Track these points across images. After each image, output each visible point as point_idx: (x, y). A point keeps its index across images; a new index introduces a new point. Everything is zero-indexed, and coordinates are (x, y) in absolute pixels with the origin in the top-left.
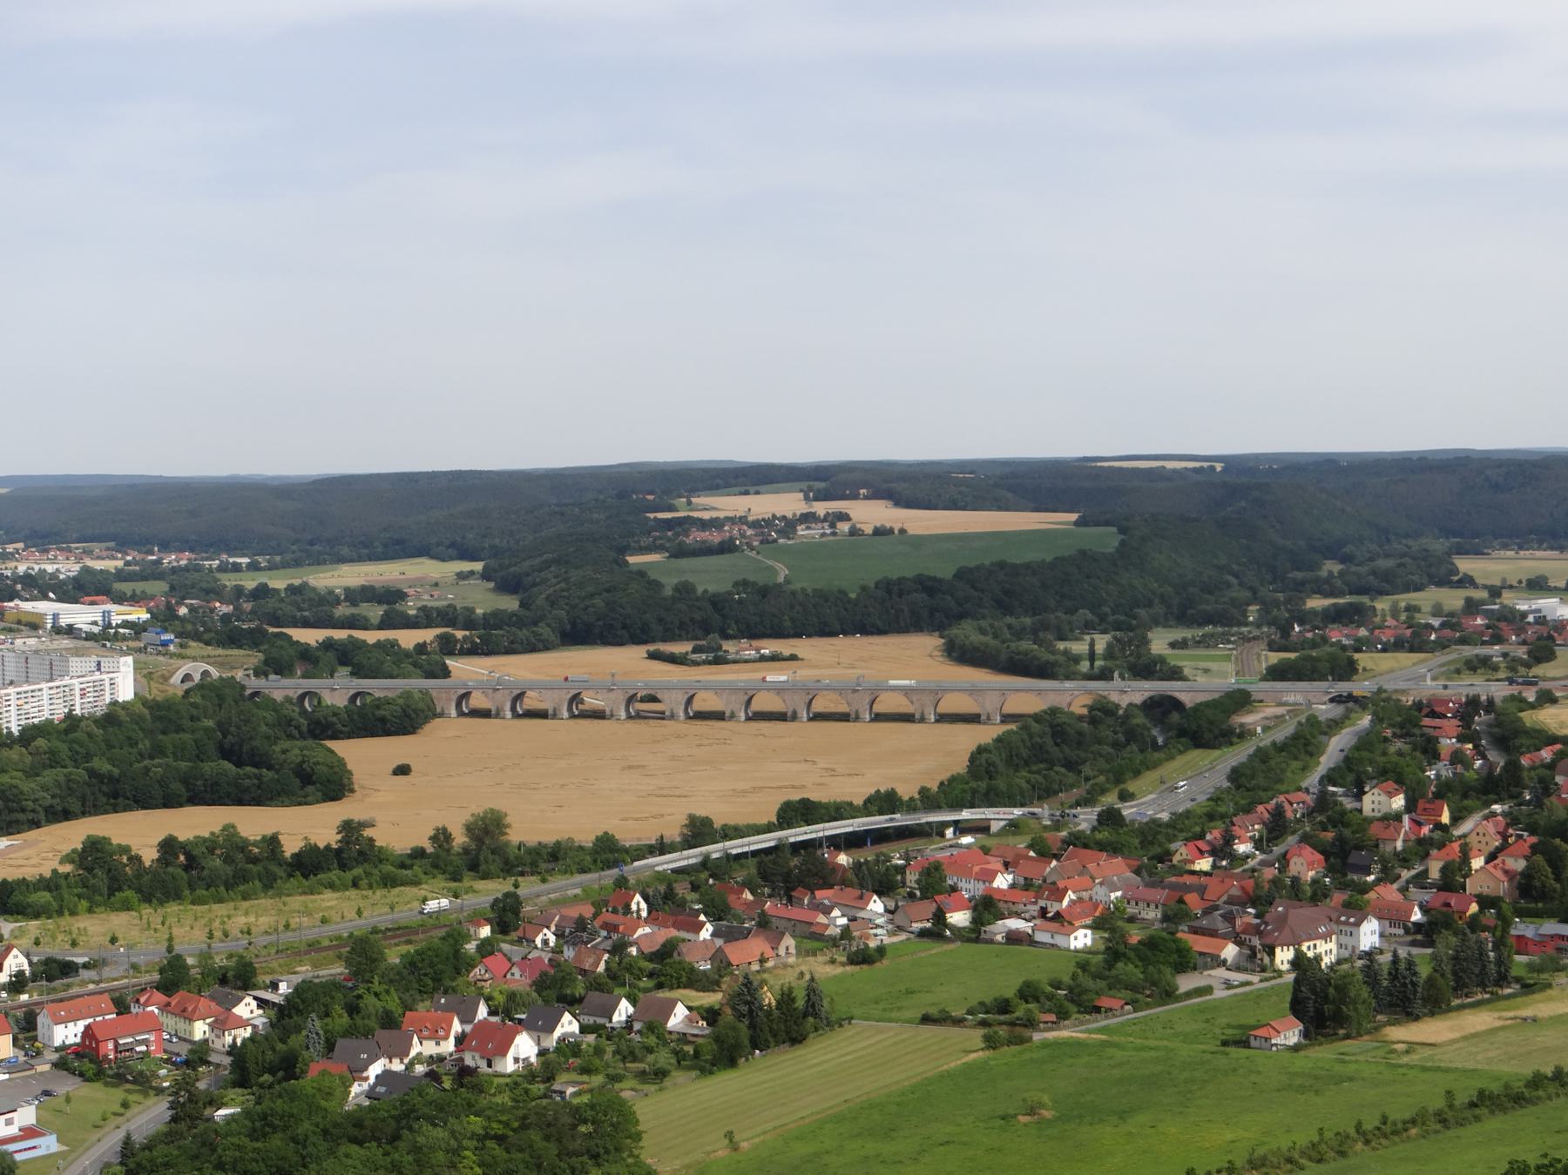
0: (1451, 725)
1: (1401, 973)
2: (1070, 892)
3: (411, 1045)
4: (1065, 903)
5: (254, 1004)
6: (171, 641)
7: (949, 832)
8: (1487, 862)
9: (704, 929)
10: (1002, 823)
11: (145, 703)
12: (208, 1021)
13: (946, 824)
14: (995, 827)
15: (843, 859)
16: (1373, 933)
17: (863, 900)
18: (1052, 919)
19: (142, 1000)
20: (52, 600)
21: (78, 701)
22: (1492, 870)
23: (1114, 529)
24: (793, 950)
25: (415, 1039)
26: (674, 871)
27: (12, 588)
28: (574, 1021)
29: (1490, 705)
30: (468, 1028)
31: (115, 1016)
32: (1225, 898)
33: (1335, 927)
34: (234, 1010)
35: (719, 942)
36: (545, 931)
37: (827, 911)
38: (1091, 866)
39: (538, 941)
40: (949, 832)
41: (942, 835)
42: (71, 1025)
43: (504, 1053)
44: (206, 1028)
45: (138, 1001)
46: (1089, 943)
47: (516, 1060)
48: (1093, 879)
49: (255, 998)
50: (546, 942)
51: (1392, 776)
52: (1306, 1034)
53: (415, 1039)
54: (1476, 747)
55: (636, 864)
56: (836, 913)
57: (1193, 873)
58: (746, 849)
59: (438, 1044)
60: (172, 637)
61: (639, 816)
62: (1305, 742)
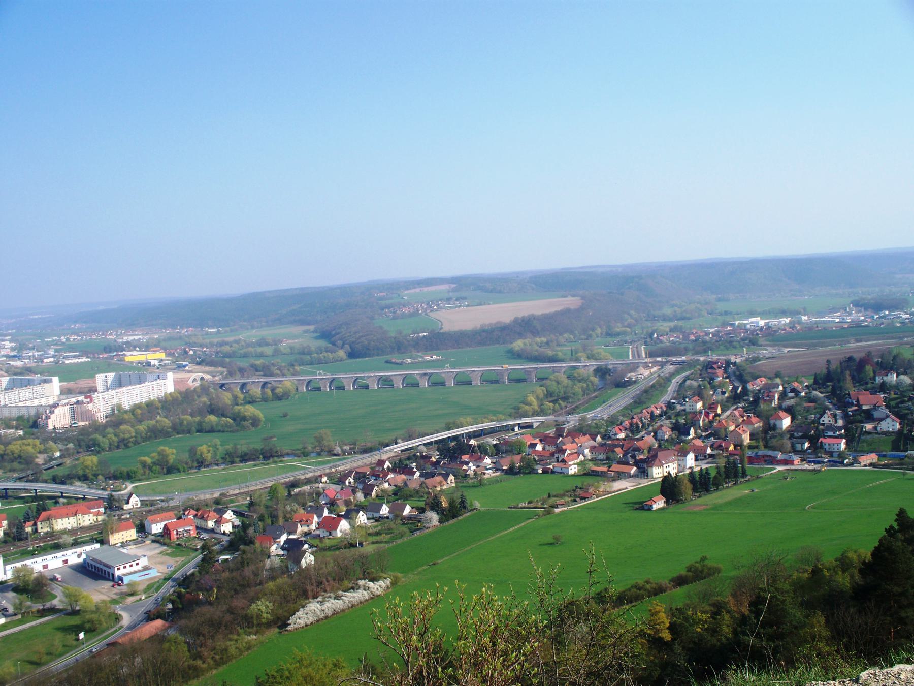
0: (720, 372)
1: (704, 474)
2: (568, 450)
3: (297, 527)
4: (566, 454)
5: (232, 513)
6: (187, 365)
7: (516, 429)
8: (736, 427)
9: (416, 475)
10: (538, 424)
11: (180, 393)
12: (214, 521)
13: (514, 425)
14: (535, 425)
15: (472, 442)
16: (692, 459)
17: (481, 459)
18: (561, 461)
19: (186, 513)
20: (137, 351)
21: (151, 392)
22: (739, 431)
23: (579, 298)
24: (453, 481)
25: (299, 525)
26: (402, 451)
27: (122, 347)
28: (364, 515)
29: (735, 364)
30: (321, 519)
31: (175, 520)
32: (631, 449)
33: (677, 458)
34: (224, 516)
35: (422, 479)
36: (350, 478)
37: (467, 464)
38: (576, 440)
39: (347, 483)
40: (516, 429)
41: (513, 430)
42: (158, 524)
43: (336, 529)
44: (213, 524)
45: (184, 514)
46: (577, 471)
47: (341, 531)
48: (577, 444)
49: (232, 511)
50: (350, 483)
51: (699, 394)
52: (667, 502)
53: (299, 525)
54: (730, 380)
55: (386, 448)
56: (471, 464)
57: (618, 439)
58: (431, 440)
59: (308, 526)
60: (188, 363)
61: (335, 457)
62: (661, 385)
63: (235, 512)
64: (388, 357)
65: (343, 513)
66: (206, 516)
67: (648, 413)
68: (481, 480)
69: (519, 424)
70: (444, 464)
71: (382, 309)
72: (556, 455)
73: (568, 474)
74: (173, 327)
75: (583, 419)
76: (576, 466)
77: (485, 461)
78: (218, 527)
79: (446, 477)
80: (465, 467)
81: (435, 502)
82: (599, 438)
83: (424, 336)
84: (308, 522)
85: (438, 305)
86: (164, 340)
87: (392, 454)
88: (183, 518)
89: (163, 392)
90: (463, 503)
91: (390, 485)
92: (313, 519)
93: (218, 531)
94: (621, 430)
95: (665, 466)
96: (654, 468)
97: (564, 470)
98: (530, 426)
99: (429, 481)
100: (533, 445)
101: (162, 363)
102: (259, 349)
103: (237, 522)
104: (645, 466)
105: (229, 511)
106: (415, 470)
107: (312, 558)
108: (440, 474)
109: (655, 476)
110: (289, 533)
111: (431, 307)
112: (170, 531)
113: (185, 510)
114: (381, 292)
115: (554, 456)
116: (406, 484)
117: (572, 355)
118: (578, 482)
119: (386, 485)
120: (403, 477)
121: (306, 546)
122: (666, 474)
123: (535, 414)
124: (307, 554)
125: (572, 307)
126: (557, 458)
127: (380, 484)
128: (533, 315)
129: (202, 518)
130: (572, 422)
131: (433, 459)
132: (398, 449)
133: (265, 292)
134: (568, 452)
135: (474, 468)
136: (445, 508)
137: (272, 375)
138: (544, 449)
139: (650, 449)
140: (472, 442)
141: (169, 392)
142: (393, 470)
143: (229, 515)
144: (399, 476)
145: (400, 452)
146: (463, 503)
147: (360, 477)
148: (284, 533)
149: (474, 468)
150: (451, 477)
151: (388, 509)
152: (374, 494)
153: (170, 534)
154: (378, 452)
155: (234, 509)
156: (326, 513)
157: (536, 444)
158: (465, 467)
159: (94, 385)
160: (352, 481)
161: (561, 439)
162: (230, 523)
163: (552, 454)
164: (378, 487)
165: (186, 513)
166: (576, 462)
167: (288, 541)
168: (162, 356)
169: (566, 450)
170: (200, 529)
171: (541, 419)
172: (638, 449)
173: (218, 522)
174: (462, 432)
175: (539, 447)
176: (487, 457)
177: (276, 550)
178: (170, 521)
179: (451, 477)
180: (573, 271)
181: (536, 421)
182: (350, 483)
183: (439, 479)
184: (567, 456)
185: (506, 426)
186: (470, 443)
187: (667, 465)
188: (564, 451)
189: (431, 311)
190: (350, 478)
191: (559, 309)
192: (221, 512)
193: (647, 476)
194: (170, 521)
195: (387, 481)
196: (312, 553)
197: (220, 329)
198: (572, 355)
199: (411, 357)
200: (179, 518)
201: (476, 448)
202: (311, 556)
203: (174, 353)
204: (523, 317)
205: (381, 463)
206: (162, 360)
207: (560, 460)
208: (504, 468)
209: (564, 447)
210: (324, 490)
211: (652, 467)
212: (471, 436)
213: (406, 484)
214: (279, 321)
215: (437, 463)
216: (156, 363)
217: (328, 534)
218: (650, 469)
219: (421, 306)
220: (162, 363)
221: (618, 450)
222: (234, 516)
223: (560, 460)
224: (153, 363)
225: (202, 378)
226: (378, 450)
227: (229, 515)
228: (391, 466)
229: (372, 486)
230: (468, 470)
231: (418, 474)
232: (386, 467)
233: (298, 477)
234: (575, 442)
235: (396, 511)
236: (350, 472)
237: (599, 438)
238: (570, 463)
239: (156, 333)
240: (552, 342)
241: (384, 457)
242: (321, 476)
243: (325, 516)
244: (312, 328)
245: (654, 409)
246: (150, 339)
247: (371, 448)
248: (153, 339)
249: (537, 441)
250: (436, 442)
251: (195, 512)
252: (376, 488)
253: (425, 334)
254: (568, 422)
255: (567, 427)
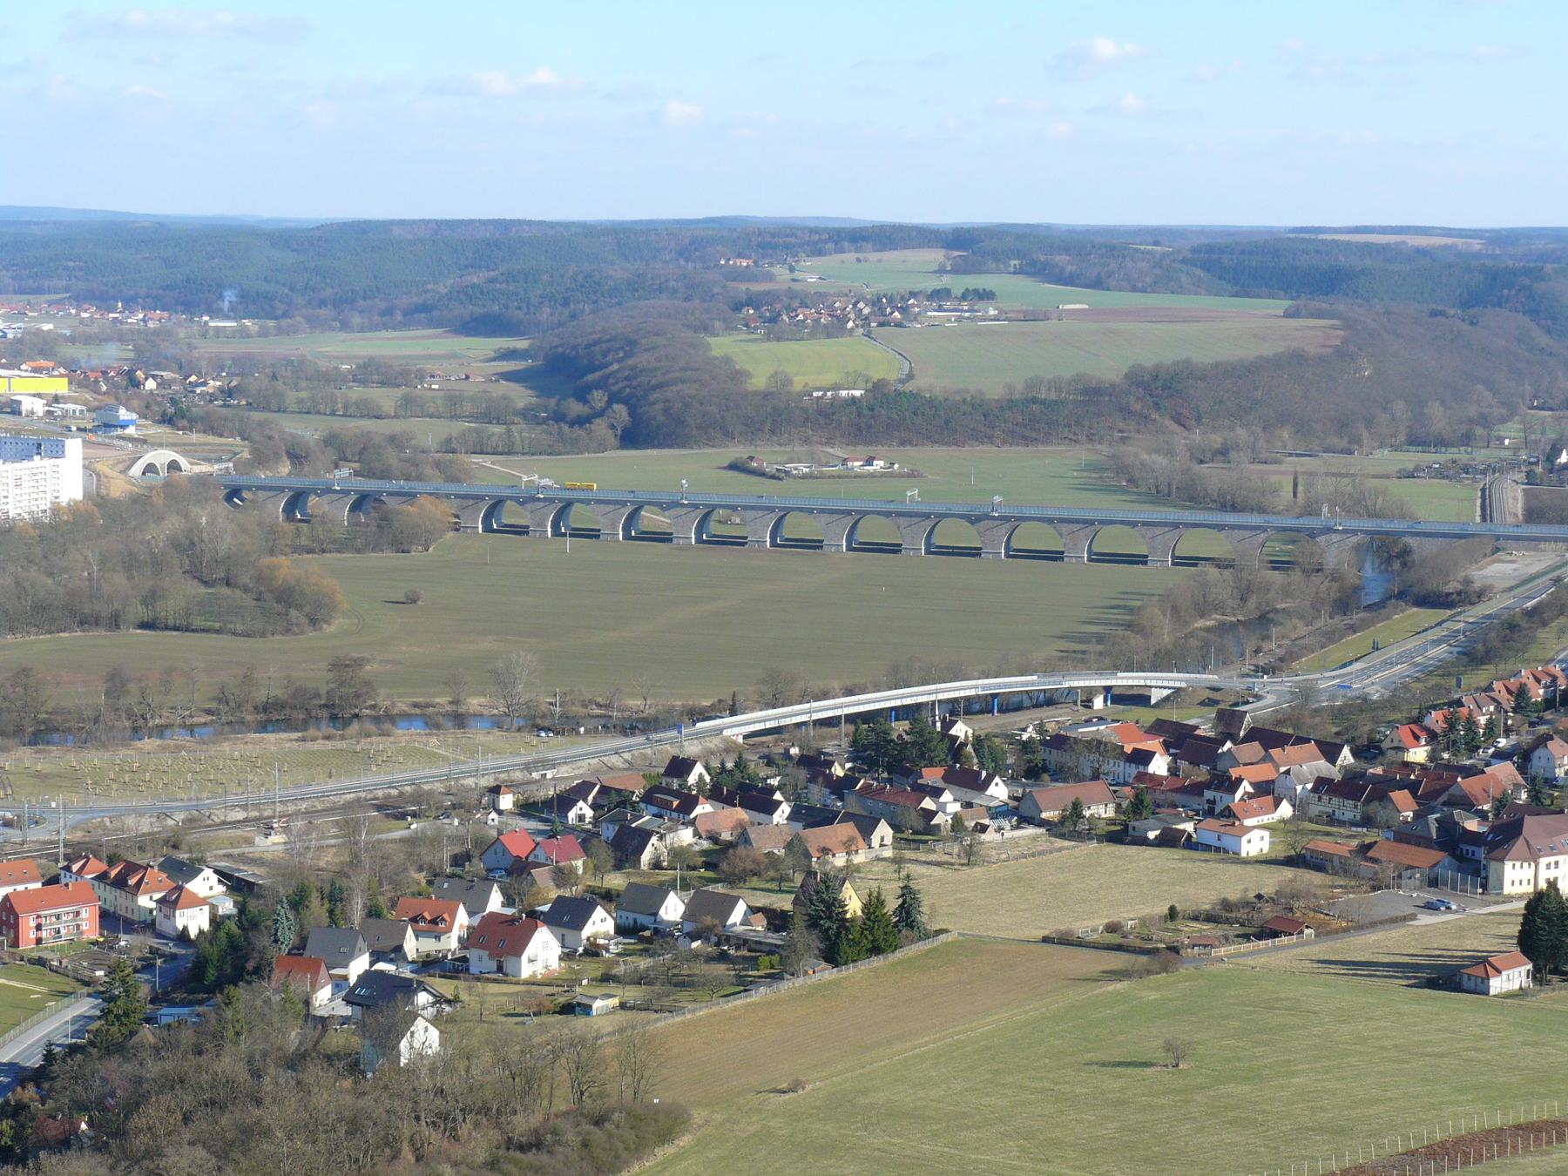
9: (779, 812)
10: (1166, 692)
12: (157, 896)
13: (1090, 693)
14: (1156, 696)
19: (75, 868)
24: (888, 840)
25: (410, 931)
30: (476, 920)
31: (39, 885)
37: (936, 793)
40: (1098, 703)
41: (1087, 703)
45: (68, 869)
48: (1277, 767)
49: (216, 871)
52: (1537, 975)
53: (410, 931)
56: (947, 797)
63: (223, 875)
64: (736, 452)
65: (546, 908)
66: (132, 881)
67: (1509, 692)
68: (971, 846)
69: (1107, 689)
70: (867, 787)
71: (738, 308)
72: (1208, 794)
73: (1237, 853)
74: (103, 300)
75: (1305, 694)
76: (1266, 834)
77: (992, 790)
78: (167, 917)
79: (867, 828)
80: (928, 803)
81: (823, 901)
82: (1346, 756)
83: (853, 398)
84: (435, 925)
85: (903, 310)
86: (72, 340)
87: (714, 743)
88: (63, 881)
89: (50, 498)
90: (908, 913)
91: (697, 834)
92: (453, 915)
93: (163, 925)
94: (1417, 738)
95: (1544, 861)
96: (1508, 865)
97: (1227, 842)
98: (1138, 699)
99: (816, 837)
100: (1144, 757)
101: (58, 409)
102: (357, 392)
103: (227, 907)
104: (1481, 853)
105: (208, 872)
106: (778, 796)
107: (434, 1034)
108: (848, 817)
109: (1508, 889)
110: (377, 956)
111: (882, 310)
112: (17, 918)
113: (70, 859)
114: (740, 256)
115: (1201, 794)
116: (744, 838)
117: (1295, 494)
118: (1271, 881)
119: (685, 836)
120: (741, 814)
121: (423, 998)
122: (1543, 885)
123: (1161, 662)
124: (420, 1023)
125: (1312, 350)
126: (1212, 802)
127: (670, 830)
128: (1187, 363)
129: (120, 883)
130: (1270, 699)
131: (838, 771)
132: (736, 730)
133: (392, 223)
134: (1246, 787)
135: (954, 807)
136: (853, 920)
137: (384, 475)
138: (1173, 770)
139: (1501, 804)
140: (960, 730)
141: (64, 500)
142: (715, 794)
143: (205, 884)
144: (729, 810)
145: (740, 740)
146: (907, 911)
147: (612, 801)
148: (361, 953)
149: (954, 807)
150: (884, 831)
151: (681, 908)
152: (646, 856)
153: (16, 927)
154: (674, 733)
155: (222, 864)
156: (495, 902)
157: (1151, 754)
158: (928, 803)
159: (93, 452)
160: (589, 813)
161: (1228, 745)
162: (206, 909)
163: (1197, 789)
164: (661, 838)
165: (75, 868)
166: (1266, 819)
167: (368, 978)
168: (60, 386)
169: (1239, 780)
170: (109, 919)
171: (1177, 679)
172: (1467, 804)
173: (170, 903)
174: (933, 698)
175: (1159, 766)
176: (997, 779)
177: (331, 1000)
178: (20, 888)
179: (884, 831)
180: (1329, 237)
181: (1159, 684)
182: (581, 818)
183: (845, 830)
184: (1242, 799)
185: (1070, 689)
186: (952, 732)
187: (1552, 859)
188: (1234, 785)
189: (881, 325)
190: (581, 804)
191: (1281, 350)
192: (183, 870)
193: (1484, 887)
194: (20, 888)
195: (692, 823)
196: (435, 1021)
197: (247, 322)
198: (1295, 494)
199: (812, 459)
200: (53, 881)
201: (969, 748)
202: (431, 1028)
203: (97, 381)
204: (1157, 367)
205: (680, 767)
206: (56, 399)
207: (1217, 811)
208: (1044, 815)
209: (1234, 773)
210: (500, 833)
211: (1501, 860)
212: (957, 709)
213: (744, 838)
214: (422, 314)
215: (849, 781)
216: (39, 407)
217: (493, 965)
218: (1493, 865)
219: (855, 305)
220: (58, 409)
221: (1401, 797)
222: (222, 888)
223: (1217, 811)
224: (27, 404)
225: (174, 466)
226: (678, 727)
227: (205, 884)
228: (707, 778)
229: (644, 836)
230: (936, 813)
231: (785, 809)
232: (692, 779)
233: (426, 787)
234: (1272, 760)
235: (703, 914)
236: (581, 791)
237: (1346, 756)
238: (1248, 822)
239: (48, 317)
240: (1237, 448)
241: (691, 749)
242: (495, 790)
243: (491, 914)
244: (522, 344)
245: (1531, 682)
246: (26, 332)
247: (656, 720)
248: (39, 332)
249: (1153, 744)
250: (851, 719)
251: (103, 866)
252: (654, 839)
253: (857, 393)
254: (1258, 697)
255: (1252, 714)
